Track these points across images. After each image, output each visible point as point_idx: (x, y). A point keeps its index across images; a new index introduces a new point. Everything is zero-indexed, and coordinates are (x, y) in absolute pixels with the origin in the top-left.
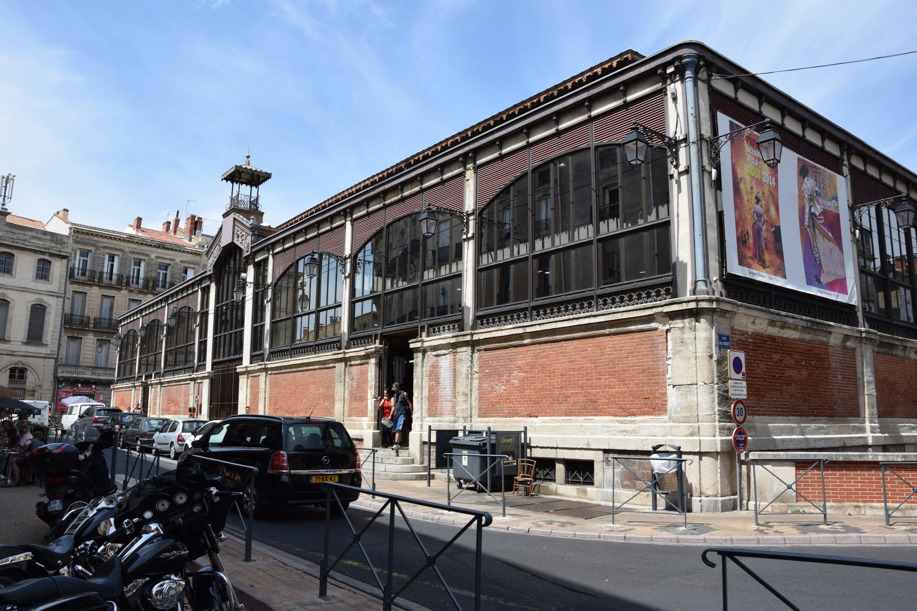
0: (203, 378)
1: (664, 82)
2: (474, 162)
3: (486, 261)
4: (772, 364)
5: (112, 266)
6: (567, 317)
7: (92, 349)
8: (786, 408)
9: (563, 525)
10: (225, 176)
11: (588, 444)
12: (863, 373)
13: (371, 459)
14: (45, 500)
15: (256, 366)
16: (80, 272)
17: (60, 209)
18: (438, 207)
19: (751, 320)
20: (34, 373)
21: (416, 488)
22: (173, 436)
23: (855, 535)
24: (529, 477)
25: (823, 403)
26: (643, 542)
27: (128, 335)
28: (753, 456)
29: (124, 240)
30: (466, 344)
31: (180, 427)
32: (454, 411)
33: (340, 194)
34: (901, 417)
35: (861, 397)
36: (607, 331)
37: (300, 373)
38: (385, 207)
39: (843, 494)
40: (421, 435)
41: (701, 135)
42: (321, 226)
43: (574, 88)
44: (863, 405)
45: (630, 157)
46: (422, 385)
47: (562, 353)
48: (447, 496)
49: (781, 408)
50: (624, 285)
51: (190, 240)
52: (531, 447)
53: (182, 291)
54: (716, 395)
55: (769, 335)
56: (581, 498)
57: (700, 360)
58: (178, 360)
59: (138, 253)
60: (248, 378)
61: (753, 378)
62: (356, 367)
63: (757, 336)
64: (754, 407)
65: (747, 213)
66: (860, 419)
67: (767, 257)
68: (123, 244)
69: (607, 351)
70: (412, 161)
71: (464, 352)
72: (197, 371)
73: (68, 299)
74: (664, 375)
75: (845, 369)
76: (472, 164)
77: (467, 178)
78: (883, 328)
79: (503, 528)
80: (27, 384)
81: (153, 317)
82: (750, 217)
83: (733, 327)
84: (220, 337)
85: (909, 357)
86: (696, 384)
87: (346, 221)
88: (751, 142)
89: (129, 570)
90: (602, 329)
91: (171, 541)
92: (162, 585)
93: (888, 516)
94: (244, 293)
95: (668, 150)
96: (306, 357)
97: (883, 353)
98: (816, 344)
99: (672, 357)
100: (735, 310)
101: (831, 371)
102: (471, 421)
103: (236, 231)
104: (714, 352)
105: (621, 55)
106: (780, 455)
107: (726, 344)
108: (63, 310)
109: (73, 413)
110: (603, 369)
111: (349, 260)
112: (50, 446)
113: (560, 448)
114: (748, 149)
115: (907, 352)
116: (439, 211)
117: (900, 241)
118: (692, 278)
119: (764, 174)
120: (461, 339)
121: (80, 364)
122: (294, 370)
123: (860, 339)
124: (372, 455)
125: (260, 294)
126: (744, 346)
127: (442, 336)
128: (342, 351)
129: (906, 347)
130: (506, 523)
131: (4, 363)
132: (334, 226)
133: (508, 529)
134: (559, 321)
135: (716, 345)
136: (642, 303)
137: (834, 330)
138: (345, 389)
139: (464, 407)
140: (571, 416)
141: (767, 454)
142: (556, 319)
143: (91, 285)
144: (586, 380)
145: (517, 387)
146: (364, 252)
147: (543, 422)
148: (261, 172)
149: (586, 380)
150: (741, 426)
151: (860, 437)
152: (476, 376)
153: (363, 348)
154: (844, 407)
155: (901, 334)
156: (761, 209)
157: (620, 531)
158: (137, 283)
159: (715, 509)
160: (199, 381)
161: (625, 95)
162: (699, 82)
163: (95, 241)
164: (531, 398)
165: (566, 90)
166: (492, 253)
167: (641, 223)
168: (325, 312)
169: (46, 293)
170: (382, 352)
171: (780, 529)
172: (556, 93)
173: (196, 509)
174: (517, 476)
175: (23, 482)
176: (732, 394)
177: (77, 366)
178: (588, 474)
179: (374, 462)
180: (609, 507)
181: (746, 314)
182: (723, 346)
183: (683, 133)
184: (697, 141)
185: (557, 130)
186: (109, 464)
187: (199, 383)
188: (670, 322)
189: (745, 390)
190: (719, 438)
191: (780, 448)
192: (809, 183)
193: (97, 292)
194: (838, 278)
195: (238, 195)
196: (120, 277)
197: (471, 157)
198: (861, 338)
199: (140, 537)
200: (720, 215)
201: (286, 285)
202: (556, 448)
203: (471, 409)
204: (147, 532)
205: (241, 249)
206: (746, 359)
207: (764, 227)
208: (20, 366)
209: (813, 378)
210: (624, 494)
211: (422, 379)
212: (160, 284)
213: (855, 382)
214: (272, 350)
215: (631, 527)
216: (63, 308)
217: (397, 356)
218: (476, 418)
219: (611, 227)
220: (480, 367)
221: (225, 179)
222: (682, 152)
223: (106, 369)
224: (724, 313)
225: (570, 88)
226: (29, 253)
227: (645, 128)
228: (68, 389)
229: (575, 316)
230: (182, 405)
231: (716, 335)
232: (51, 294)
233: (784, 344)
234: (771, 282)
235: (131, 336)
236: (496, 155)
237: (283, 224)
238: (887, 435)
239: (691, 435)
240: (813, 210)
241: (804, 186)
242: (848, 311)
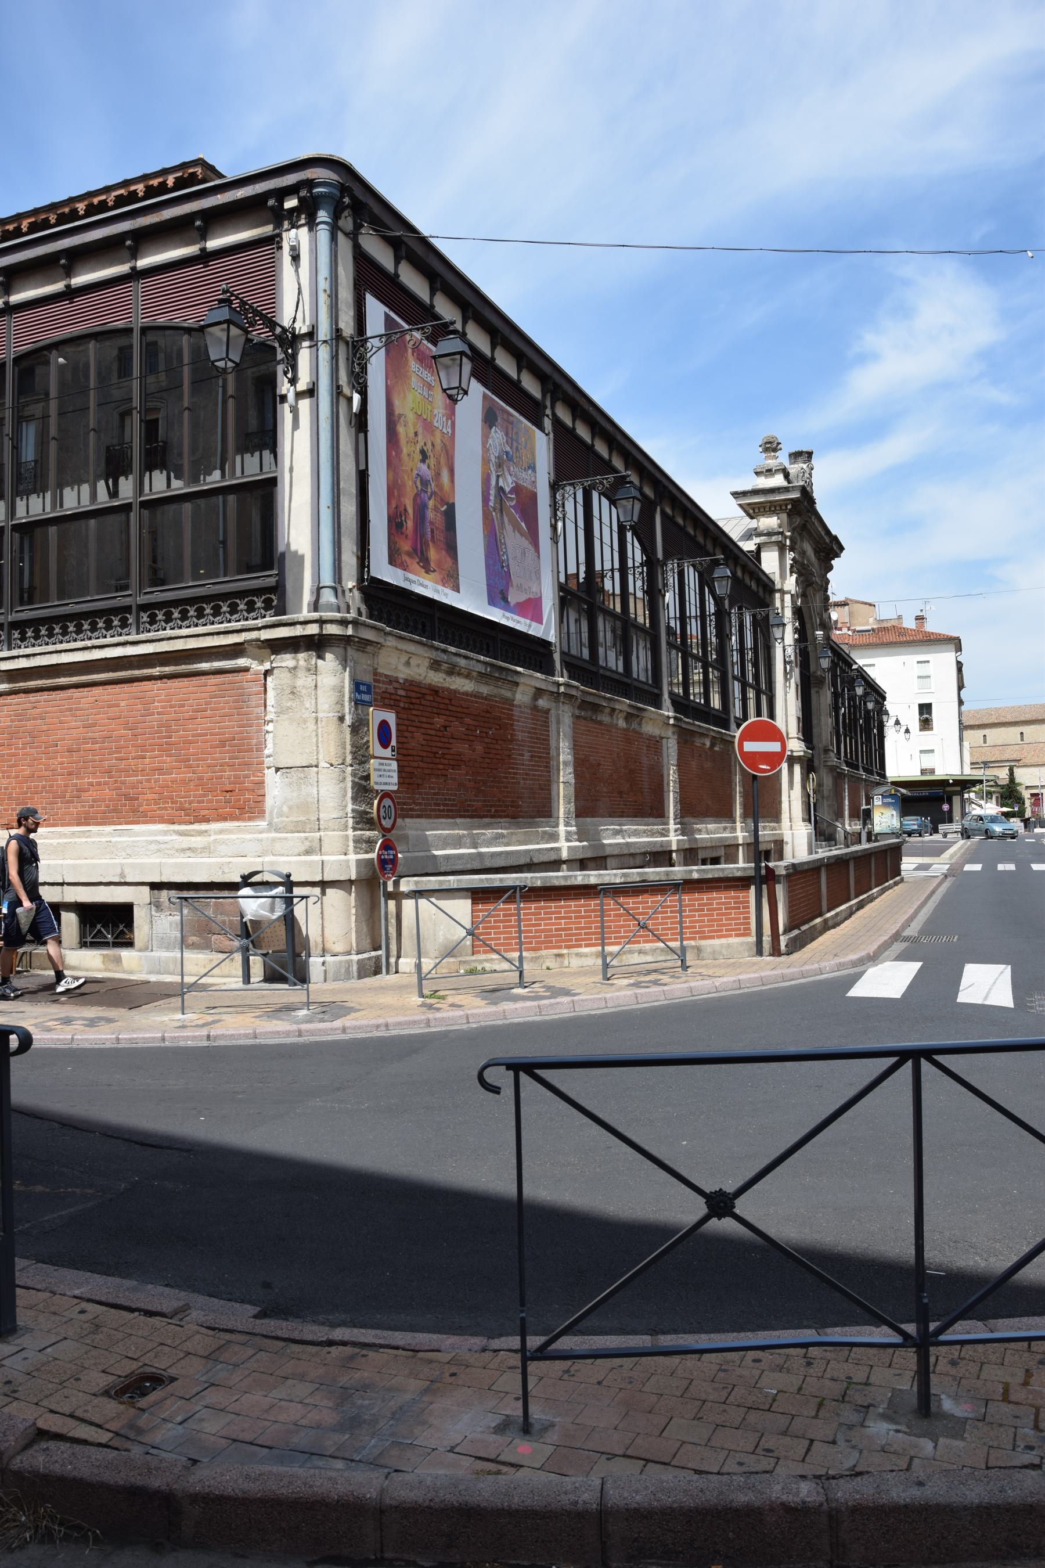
1: (278, 225)
4: (433, 732)
6: (79, 644)
8: (452, 805)
9: (92, 1023)
11: (122, 875)
12: (558, 749)
19: (404, 658)
23: (565, 999)
25: (504, 797)
26: (241, 1042)
28: (407, 885)
34: (603, 816)
35: (554, 786)
36: (156, 671)
39: (540, 937)
41: (338, 330)
44: (556, 798)
45: (215, 353)
47: (70, 710)
49: (444, 805)
50: (189, 588)
54: (349, 784)
55: (430, 685)
56: (110, 971)
57: (323, 723)
61: (404, 755)
63: (411, 685)
64: (404, 804)
65: (406, 478)
66: (552, 820)
67: (433, 554)
69: (157, 707)
74: (260, 750)
75: (534, 743)
78: (585, 679)
82: (410, 483)
83: (376, 669)
85: (617, 725)
86: (317, 766)
88: (418, 355)
93: (606, 966)
95: (279, 350)
97: (585, 719)
98: (496, 701)
99: (275, 718)
100: (381, 640)
101: (517, 745)
104: (347, 710)
105: (184, 166)
106: (449, 881)
107: (366, 697)
113: (69, 884)
114: (413, 365)
115: (614, 717)
117: (612, 547)
118: (313, 581)
119: (436, 412)
123: (556, 696)
126: (392, 703)
129: (613, 710)
135: (350, 698)
136: (222, 623)
137: (522, 680)
140: (88, 824)
141: (429, 881)
144: (117, 759)
149: (117, 759)
150: (389, 836)
151: (552, 849)
154: (531, 803)
155: (615, 691)
156: (429, 472)
157: (197, 1026)
159: (348, 976)
162: (340, 235)
167: (214, 479)
171: (457, 999)
176: (376, 783)
178: (121, 927)
180: (177, 983)
181: (397, 649)
182: (361, 701)
183: (308, 322)
184: (332, 339)
185: (68, 286)
188: (273, 657)
189: (395, 775)
190: (353, 857)
191: (442, 870)
192: (497, 435)
194: (531, 596)
198: (558, 693)
200: (363, 477)
202: (62, 884)
206: (397, 724)
207: (431, 503)
209: (491, 756)
210: (197, 962)
213: (547, 762)
215: (216, 1017)
219: (158, 484)
222: (304, 356)
224: (363, 644)
225: (82, 212)
227: (243, 303)
231: (350, 682)
233: (450, 700)
234: (436, 597)
238: (585, 843)
239: (308, 852)
240: (501, 484)
241: (490, 441)
242: (542, 650)
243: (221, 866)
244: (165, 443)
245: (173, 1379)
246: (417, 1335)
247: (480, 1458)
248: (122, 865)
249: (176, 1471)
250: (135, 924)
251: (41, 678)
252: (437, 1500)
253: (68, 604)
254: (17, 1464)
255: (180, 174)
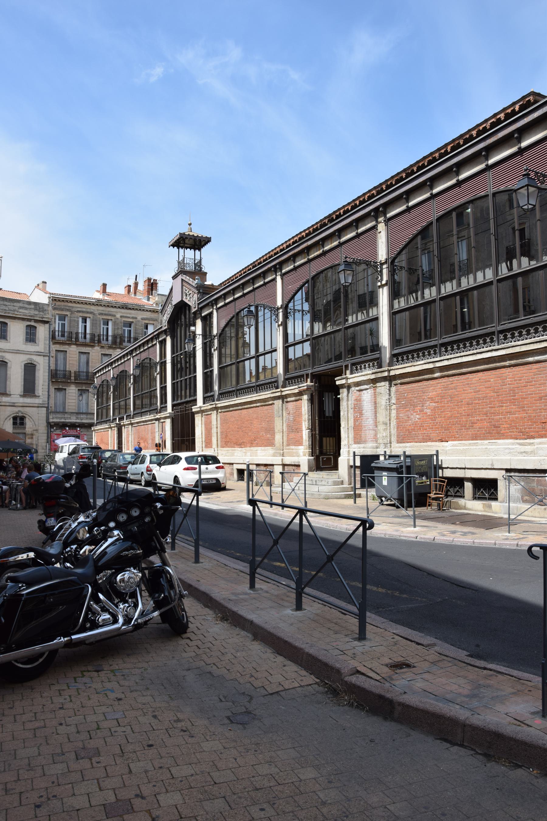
0: (165, 418)
2: (385, 215)
3: (401, 303)
5: (85, 327)
7: (74, 398)
9: (465, 534)
10: (171, 243)
11: (492, 465)
13: (303, 481)
14: (43, 518)
15: (208, 406)
16: (60, 334)
17: (40, 282)
18: (354, 259)
20: (31, 420)
21: (344, 505)
22: (142, 468)
24: (442, 494)
27: (103, 385)
29: (93, 304)
30: (384, 379)
31: (148, 460)
32: (376, 439)
33: (272, 250)
36: (507, 363)
37: (245, 410)
38: (310, 261)
40: (348, 460)
42: (255, 281)
43: (478, 135)
45: (523, 202)
46: (348, 417)
47: (468, 384)
48: (366, 511)
51: (148, 300)
52: (442, 468)
53: (143, 344)
56: (486, 511)
58: (144, 403)
59: (105, 315)
60: (202, 416)
62: (292, 403)
68: (93, 307)
70: (334, 216)
71: (383, 386)
72: (160, 412)
73: (53, 357)
76: (383, 218)
77: (379, 231)
79: (412, 537)
80: (27, 429)
81: (121, 368)
84: (177, 382)
87: (276, 275)
89: (100, 564)
90: (503, 362)
91: (129, 543)
92: (124, 575)
94: (194, 344)
96: (249, 396)
102: (391, 446)
103: (184, 290)
105: (524, 98)
108: (49, 367)
109: (64, 451)
110: (505, 397)
111: (281, 310)
112: (43, 476)
113: (468, 469)
116: (358, 263)
120: (380, 375)
121: (66, 411)
122: (240, 407)
124: (303, 478)
125: (208, 344)
127: (363, 373)
128: (279, 390)
130: (416, 533)
131: (8, 413)
132: (266, 280)
133: (416, 538)
134: (465, 356)
138: (283, 423)
139: (384, 435)
140: (477, 440)
142: (462, 354)
143: (69, 344)
145: (429, 416)
146: (294, 302)
147: (453, 446)
148: (202, 236)
152: (394, 407)
153: (296, 387)
157: (514, 539)
158: (107, 340)
160: (162, 421)
161: (520, 142)
163: (69, 307)
164: (442, 425)
165: (472, 138)
166: (414, 295)
168: (270, 354)
169: (35, 353)
170: (313, 389)
172: (461, 142)
173: (147, 520)
174: (430, 493)
175: (29, 506)
177: (64, 413)
178: (492, 490)
179: (305, 484)
185: (458, 180)
186: (90, 490)
187: (162, 422)
193: (75, 349)
195: (184, 259)
196: (93, 335)
197: (381, 211)
199: (107, 541)
201: (229, 335)
202: (465, 468)
203: (390, 436)
204: (111, 537)
205: (189, 306)
208: (20, 415)
211: (348, 411)
212: (126, 340)
214: (220, 392)
216: (49, 365)
217: (327, 391)
218: (394, 444)
220: (397, 399)
221: (171, 245)
223: (87, 414)
225: (475, 135)
226: (19, 321)
228: (58, 432)
229: (478, 351)
230: (150, 442)
232: (39, 354)
235: (105, 385)
236: (404, 208)
237: (226, 281)
243: (540, 461)
244: (529, 240)
245: (414, 667)
246: (524, 673)
247: (516, 719)
248: (492, 460)
249: (397, 694)
250: (499, 489)
251: (454, 369)
252: (487, 727)
253: (465, 333)
254: (346, 679)
255: (521, 103)
